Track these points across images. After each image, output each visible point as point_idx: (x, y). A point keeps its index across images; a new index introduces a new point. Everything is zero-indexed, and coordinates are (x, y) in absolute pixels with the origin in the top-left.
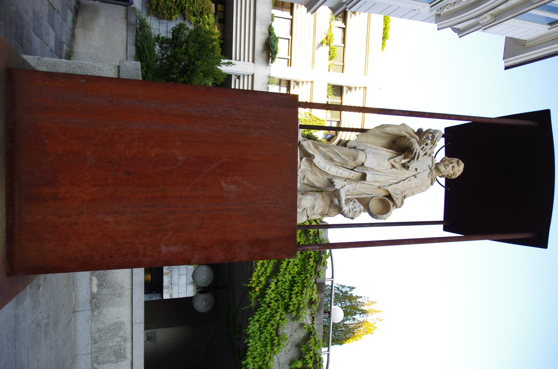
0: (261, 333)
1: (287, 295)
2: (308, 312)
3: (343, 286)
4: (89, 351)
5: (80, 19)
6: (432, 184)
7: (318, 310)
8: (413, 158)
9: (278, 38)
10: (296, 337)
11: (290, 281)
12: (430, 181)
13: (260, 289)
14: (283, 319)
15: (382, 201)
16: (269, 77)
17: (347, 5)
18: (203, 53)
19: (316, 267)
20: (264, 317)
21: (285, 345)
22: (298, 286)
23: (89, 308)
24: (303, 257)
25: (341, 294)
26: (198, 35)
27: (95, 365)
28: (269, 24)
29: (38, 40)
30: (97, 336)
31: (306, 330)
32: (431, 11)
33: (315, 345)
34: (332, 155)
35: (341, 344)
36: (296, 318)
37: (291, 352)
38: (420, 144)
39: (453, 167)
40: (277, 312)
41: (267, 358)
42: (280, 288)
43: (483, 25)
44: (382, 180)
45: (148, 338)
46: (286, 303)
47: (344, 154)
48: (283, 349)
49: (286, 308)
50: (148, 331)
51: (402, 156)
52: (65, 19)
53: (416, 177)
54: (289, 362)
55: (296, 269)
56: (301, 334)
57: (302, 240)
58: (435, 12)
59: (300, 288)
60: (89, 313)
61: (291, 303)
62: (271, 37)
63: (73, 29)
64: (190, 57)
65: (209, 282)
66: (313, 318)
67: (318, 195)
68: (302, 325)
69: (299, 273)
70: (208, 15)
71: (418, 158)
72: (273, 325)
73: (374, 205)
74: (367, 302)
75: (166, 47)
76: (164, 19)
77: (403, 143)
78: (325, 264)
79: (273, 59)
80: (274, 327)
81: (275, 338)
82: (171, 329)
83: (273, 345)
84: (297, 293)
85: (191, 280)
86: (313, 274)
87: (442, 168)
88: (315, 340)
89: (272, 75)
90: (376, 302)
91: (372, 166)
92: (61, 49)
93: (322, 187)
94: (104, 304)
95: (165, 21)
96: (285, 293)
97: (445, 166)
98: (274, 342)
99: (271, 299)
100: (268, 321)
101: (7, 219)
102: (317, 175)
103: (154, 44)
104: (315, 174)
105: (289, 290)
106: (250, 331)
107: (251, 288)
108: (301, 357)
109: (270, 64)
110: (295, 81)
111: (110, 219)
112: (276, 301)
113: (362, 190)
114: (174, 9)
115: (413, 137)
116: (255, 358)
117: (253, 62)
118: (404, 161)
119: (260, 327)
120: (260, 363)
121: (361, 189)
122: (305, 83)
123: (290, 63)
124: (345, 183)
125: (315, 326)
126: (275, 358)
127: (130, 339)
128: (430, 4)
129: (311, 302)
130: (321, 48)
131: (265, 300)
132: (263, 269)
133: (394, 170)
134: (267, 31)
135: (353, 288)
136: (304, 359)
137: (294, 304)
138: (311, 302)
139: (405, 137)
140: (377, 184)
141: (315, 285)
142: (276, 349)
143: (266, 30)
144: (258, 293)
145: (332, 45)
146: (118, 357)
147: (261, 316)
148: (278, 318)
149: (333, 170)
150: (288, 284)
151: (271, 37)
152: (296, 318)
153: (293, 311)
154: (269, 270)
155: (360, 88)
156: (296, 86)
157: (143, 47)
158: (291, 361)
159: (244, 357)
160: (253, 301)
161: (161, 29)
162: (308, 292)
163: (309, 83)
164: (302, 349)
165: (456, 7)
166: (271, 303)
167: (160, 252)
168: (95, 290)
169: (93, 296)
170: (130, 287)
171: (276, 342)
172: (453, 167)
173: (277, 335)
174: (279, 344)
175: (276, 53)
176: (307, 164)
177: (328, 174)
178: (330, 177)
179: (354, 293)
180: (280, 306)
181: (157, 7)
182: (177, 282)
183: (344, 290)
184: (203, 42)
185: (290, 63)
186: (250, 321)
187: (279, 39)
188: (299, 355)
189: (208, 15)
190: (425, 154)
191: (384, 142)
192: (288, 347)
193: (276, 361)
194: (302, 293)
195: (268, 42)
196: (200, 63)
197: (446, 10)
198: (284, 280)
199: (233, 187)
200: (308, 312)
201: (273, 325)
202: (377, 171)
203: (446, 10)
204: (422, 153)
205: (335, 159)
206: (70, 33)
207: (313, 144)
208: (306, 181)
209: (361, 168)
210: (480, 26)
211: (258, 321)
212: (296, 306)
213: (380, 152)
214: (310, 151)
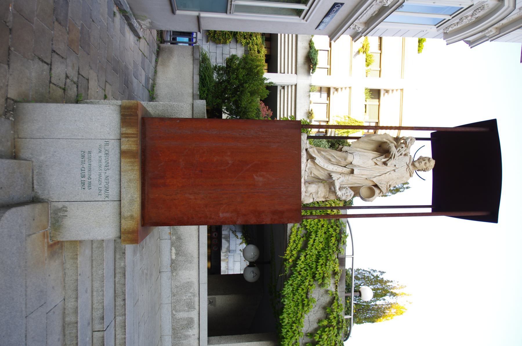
0: (294, 295)
1: (314, 266)
2: (332, 281)
3: (374, 271)
4: (170, 302)
5: (160, 59)
6: (411, 176)
7: (341, 280)
8: (391, 158)
9: (318, 51)
10: (323, 301)
11: (317, 255)
12: (409, 174)
13: (293, 261)
14: (311, 285)
15: (370, 189)
16: (311, 86)
17: (362, 33)
18: (250, 77)
19: (338, 245)
20: (296, 282)
21: (314, 306)
22: (323, 259)
23: (170, 270)
24: (326, 236)
25: (372, 277)
26: (246, 63)
27: (174, 312)
28: (309, 39)
29: (136, 80)
30: (175, 291)
31: (330, 295)
32: (438, 31)
33: (338, 308)
34: (330, 157)
35: (373, 322)
36: (322, 285)
37: (319, 312)
38: (396, 147)
39: (426, 163)
40: (306, 279)
41: (299, 315)
42: (308, 260)
43: (490, 37)
44: (367, 173)
45: (210, 303)
46: (313, 273)
47: (338, 157)
48: (312, 310)
49: (314, 277)
50: (210, 297)
51: (384, 156)
52: (151, 62)
54: (317, 321)
55: (321, 246)
56: (327, 299)
57: (325, 223)
59: (324, 261)
60: (169, 274)
61: (317, 272)
62: (311, 51)
63: (156, 67)
64: (240, 80)
65: (255, 259)
66: (336, 286)
67: (321, 185)
68: (327, 292)
69: (323, 249)
70: (256, 37)
71: (394, 157)
72: (303, 289)
73: (364, 191)
74: (398, 287)
75: (222, 74)
76: (220, 43)
77: (385, 147)
78: (344, 243)
79: (314, 70)
80: (304, 291)
81: (305, 299)
82: (227, 296)
83: (303, 305)
84: (322, 264)
85: (243, 259)
86: (335, 249)
87: (417, 164)
88: (338, 303)
89: (313, 84)
90: (405, 286)
91: (358, 164)
92: (148, 83)
93: (324, 179)
94: (180, 267)
95: (221, 45)
96: (313, 264)
97: (419, 163)
98: (304, 303)
99: (301, 269)
100: (299, 286)
101: (142, 196)
103: (213, 73)
104: (319, 170)
105: (315, 262)
106: (285, 293)
107: (286, 260)
108: (327, 317)
109: (311, 74)
110: (334, 88)
111: (192, 197)
112: (305, 270)
113: (354, 181)
114: (228, 34)
115: (392, 143)
116: (289, 314)
117: (296, 73)
118: (384, 160)
119: (293, 290)
120: (294, 319)
121: (352, 180)
122: (344, 89)
123: (329, 72)
124: (341, 176)
125: (338, 293)
126: (306, 316)
127: (198, 295)
128: (451, 15)
129: (335, 273)
130: (358, 56)
131: (296, 268)
132: (295, 245)
133: (377, 166)
134: (307, 46)
135: (383, 272)
136: (329, 319)
137: (320, 273)
138: (335, 273)
139: (386, 142)
140: (365, 177)
141: (337, 260)
142: (306, 308)
143: (306, 45)
144: (291, 264)
145: (369, 53)
146: (189, 308)
147: (293, 281)
148: (307, 284)
149: (330, 167)
150: (314, 257)
151: (311, 51)
152: (322, 285)
153: (319, 279)
154: (299, 246)
155: (397, 90)
156: (336, 92)
157: (205, 76)
158: (319, 320)
159: (282, 313)
160: (287, 269)
161: (218, 52)
162: (330, 264)
163: (348, 89)
164: (327, 310)
165: (459, 26)
166: (301, 271)
167: (219, 216)
168: (174, 257)
169: (173, 262)
170: (197, 256)
171: (306, 302)
172: (426, 163)
173: (307, 297)
174: (308, 305)
175: (316, 64)
176: (312, 163)
177: (327, 170)
178: (329, 172)
179: (385, 277)
180: (308, 274)
181: (214, 35)
182: (233, 268)
183: (375, 274)
184: (250, 68)
185: (329, 72)
186: (285, 285)
187: (319, 52)
188: (325, 316)
189: (256, 37)
190: (401, 155)
191: (372, 146)
192: (317, 308)
193: (307, 319)
194: (326, 265)
195: (309, 56)
196: (247, 86)
197: (450, 29)
198: (311, 254)
199: (261, 179)
200: (332, 281)
201: (303, 289)
202: (363, 167)
203: (450, 29)
204: (397, 154)
205: (332, 160)
206: (153, 71)
207: (317, 150)
208: (313, 175)
209: (351, 165)
210: (488, 38)
211: (291, 285)
212: (322, 275)
213: (365, 154)
214: (314, 155)
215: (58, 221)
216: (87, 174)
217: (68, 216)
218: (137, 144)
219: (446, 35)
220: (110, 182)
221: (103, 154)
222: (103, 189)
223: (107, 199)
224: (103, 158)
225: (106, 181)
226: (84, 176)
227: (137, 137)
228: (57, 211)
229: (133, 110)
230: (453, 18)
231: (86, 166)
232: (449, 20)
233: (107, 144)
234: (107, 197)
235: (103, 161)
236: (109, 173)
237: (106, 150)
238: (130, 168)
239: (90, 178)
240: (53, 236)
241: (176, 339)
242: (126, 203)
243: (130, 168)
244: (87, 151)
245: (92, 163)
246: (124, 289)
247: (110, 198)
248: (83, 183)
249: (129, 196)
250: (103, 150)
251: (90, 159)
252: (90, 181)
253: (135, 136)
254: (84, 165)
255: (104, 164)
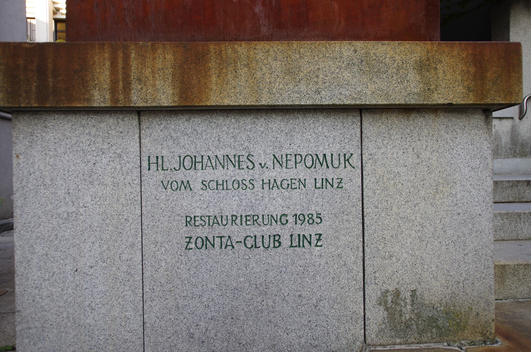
215: (432, 320)
216: (267, 230)
217: (413, 287)
218: (154, 50)
220: (295, 149)
221: (196, 177)
222: (321, 173)
223: (355, 161)
224: (209, 174)
225: (291, 163)
226: (277, 239)
227: (126, 49)
228: (396, 323)
229: (21, 62)
231: (237, 232)
233: (159, 162)
234: (347, 160)
235: (219, 174)
236: (262, 153)
237: (182, 164)
238: (243, 71)
239: (282, 220)
240: (483, 334)
241: (499, 151)
242: (372, 87)
243: (243, 71)
244: (185, 231)
245: (228, 213)
246: (506, 185)
247: (353, 148)
248: (302, 241)
249: (347, 75)
250: (180, 176)
251: (215, 220)
252: (291, 219)
253: (121, 54)
254: (235, 239)
255: (231, 173)
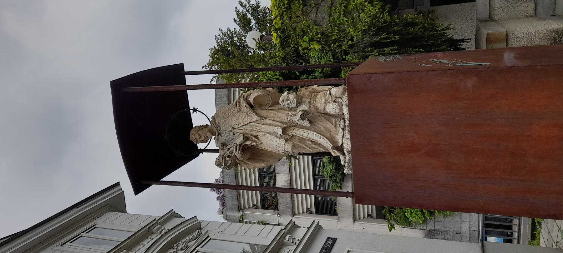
43: (156, 224)
53: (233, 128)
58: (203, 232)
102: (325, 128)
118: (248, 143)
133: (255, 134)
149: (312, 135)
203: (195, 234)
219: (198, 227)
230: (195, 249)
232: (198, 246)
